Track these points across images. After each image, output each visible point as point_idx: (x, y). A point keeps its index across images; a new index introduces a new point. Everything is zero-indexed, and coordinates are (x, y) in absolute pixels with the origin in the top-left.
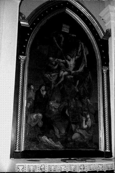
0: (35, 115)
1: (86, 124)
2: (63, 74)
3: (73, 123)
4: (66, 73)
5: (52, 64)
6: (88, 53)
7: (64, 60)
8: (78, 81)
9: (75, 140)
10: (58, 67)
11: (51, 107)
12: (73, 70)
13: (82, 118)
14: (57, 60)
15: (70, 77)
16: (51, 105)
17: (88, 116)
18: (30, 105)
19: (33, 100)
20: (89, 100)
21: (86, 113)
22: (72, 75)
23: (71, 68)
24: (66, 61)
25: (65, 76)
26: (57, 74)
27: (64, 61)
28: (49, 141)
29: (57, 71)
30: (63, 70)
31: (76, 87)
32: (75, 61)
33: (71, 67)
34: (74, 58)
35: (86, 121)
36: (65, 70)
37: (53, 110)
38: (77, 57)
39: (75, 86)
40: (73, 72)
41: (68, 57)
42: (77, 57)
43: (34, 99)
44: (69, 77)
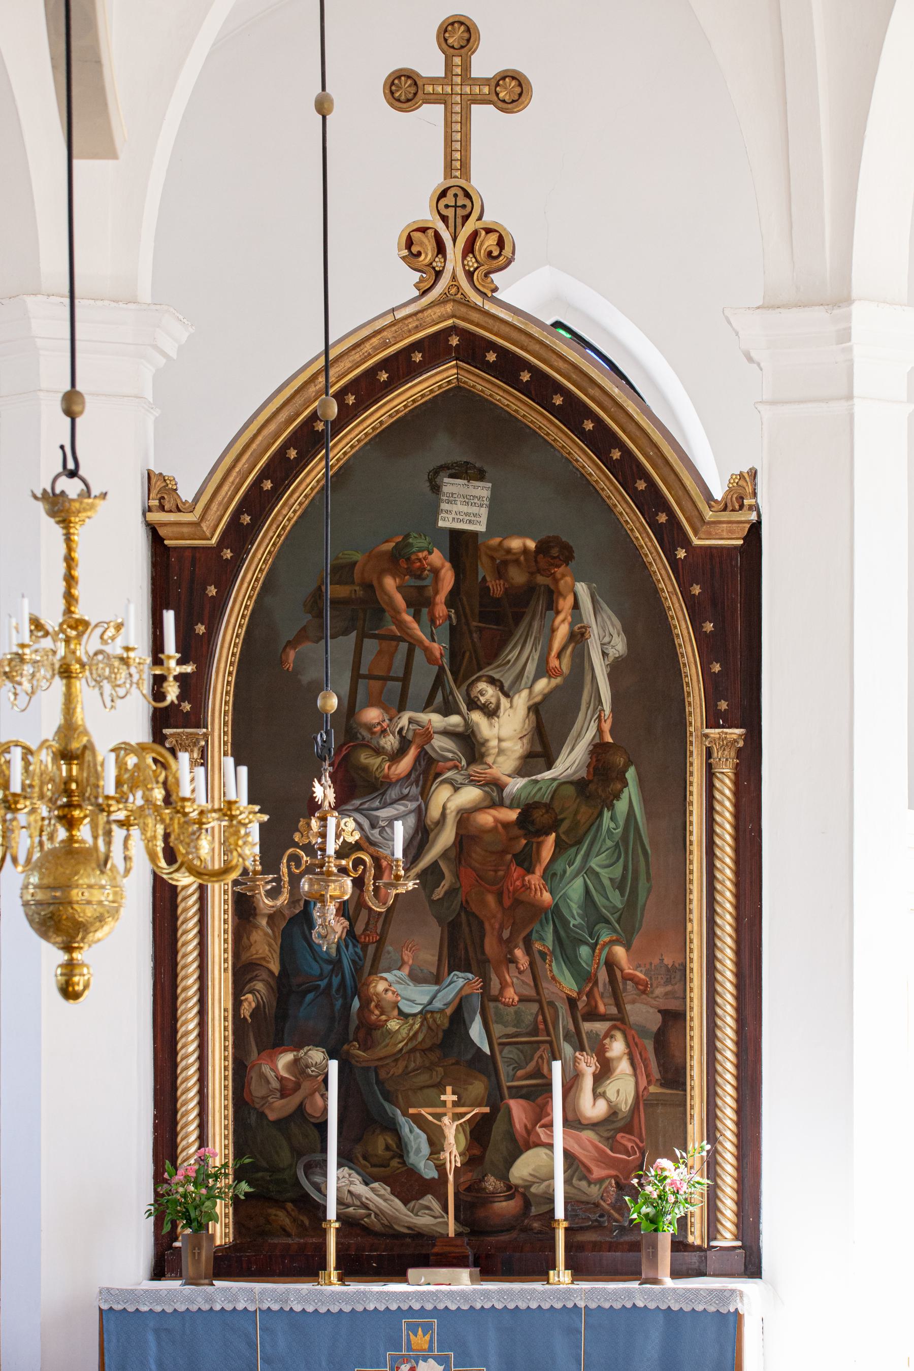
0: (285, 1059)
1: (596, 1095)
2: (452, 806)
3: (517, 1093)
4: (470, 795)
5: (378, 751)
6: (619, 646)
7: (458, 712)
8: (420, 1329)
9: (528, 1187)
10: (417, 759)
11: (377, 1006)
12: (520, 772)
13: (575, 1058)
14: (411, 721)
15: (496, 820)
16: (377, 994)
17: (617, 1047)
18: (254, 1005)
19: (271, 972)
20: (620, 951)
21: (600, 1027)
22: (511, 807)
23: (501, 759)
24: (467, 723)
25: (465, 816)
26: (412, 805)
27: (455, 719)
28: (371, 1195)
29: (415, 790)
30: (449, 781)
31: (535, 879)
32: (535, 709)
33: (501, 752)
34: (525, 693)
35: (600, 1077)
36: (459, 778)
37: (393, 1025)
38: (542, 685)
39: (530, 870)
40: (516, 785)
41: (482, 693)
42: (542, 685)
43: (275, 968)
44: (486, 819)
